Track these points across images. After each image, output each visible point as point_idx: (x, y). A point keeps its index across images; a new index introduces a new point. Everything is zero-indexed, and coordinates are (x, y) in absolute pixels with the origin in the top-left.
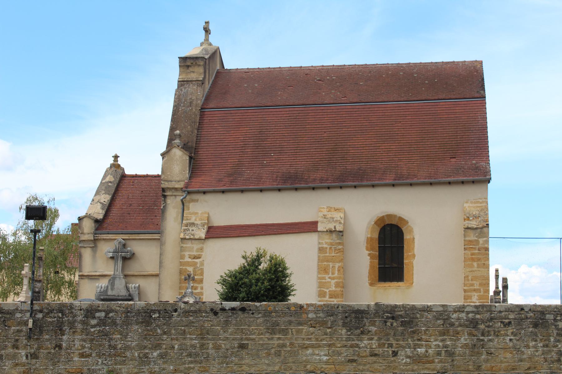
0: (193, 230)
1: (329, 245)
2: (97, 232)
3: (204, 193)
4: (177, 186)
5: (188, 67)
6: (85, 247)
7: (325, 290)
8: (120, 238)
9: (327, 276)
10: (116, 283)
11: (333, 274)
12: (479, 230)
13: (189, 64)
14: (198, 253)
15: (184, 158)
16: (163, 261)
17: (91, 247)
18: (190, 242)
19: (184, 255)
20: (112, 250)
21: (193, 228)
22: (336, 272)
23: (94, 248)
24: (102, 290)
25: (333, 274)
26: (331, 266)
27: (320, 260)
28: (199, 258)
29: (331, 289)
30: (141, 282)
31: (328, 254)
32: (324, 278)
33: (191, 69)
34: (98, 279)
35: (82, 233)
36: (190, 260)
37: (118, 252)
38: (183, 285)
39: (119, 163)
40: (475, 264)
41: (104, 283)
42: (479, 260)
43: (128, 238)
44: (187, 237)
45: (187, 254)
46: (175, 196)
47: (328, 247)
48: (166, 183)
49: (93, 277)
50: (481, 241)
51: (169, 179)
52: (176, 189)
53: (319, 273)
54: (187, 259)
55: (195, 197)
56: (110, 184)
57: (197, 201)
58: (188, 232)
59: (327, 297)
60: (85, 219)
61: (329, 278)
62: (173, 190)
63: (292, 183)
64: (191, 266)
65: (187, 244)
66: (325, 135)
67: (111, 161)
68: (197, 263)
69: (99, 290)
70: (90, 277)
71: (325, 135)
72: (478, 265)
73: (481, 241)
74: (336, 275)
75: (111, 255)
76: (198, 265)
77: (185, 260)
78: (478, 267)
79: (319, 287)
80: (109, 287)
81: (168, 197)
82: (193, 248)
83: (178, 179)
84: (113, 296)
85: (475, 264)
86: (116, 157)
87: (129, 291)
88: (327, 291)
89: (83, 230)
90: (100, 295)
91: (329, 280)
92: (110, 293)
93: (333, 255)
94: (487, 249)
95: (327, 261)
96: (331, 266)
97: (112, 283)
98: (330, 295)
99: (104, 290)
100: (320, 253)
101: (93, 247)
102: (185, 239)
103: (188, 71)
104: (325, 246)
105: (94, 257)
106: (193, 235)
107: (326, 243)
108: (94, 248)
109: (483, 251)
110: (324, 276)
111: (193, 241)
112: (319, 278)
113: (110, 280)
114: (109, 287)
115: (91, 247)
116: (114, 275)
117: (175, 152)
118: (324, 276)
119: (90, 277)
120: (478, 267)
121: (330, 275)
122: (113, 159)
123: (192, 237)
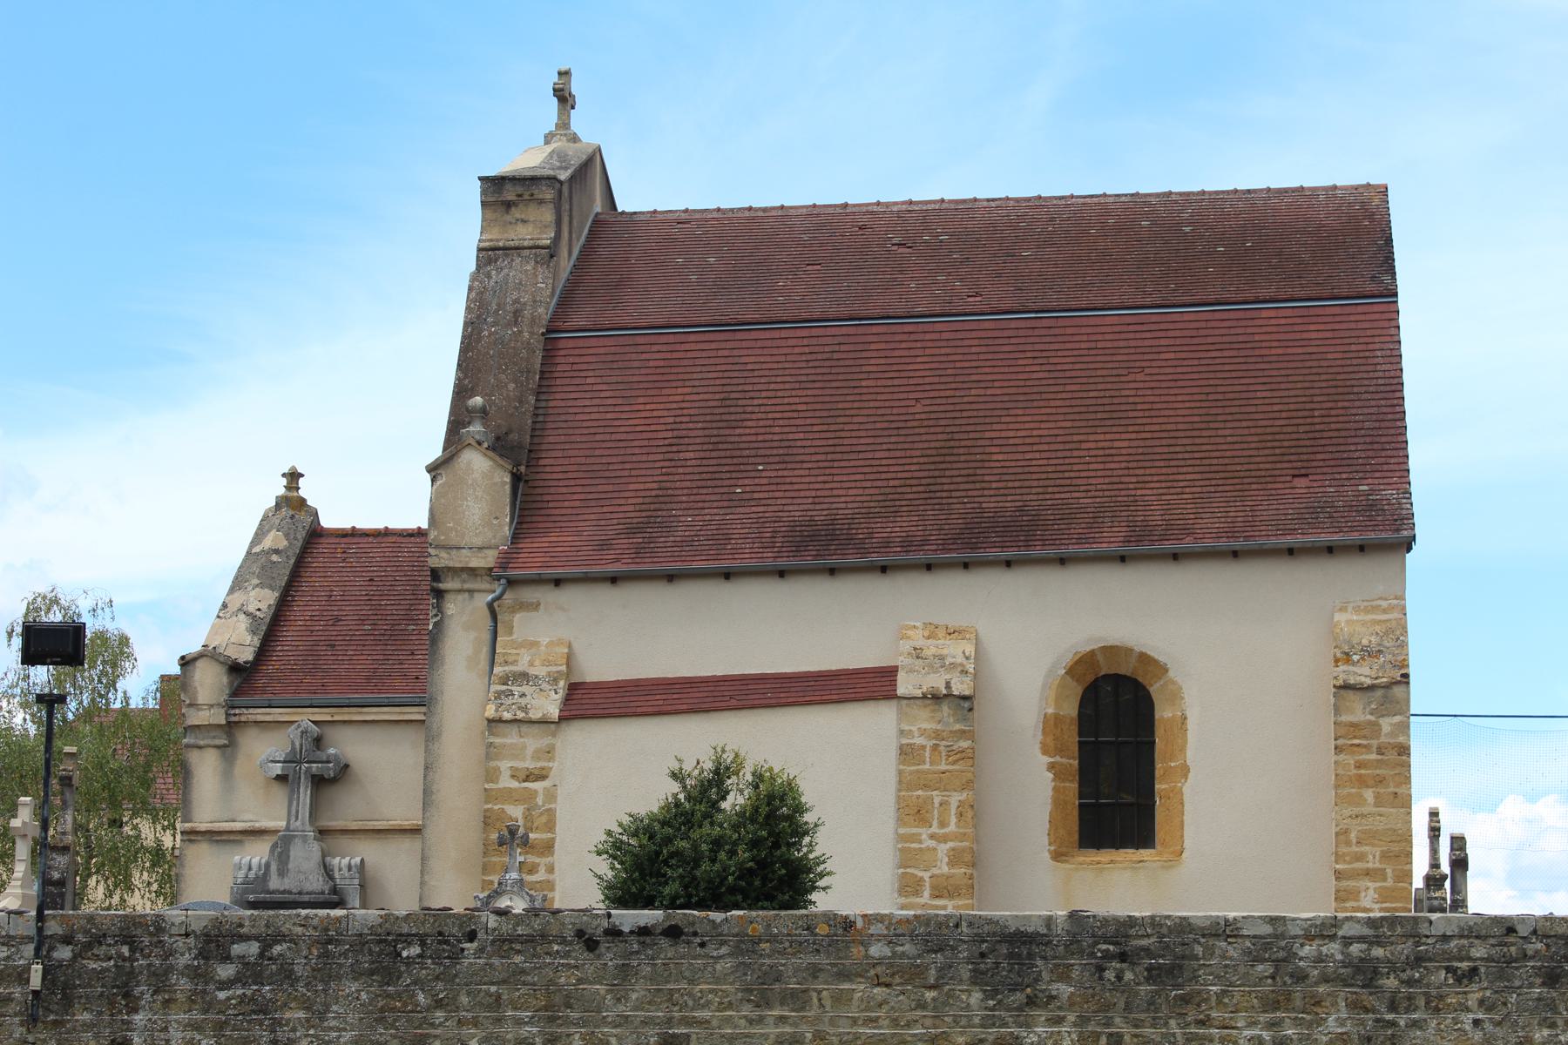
0: (523, 695)
1: (930, 738)
2: (238, 700)
3: (558, 582)
4: (474, 563)
5: (508, 205)
6: (200, 747)
8: (305, 717)
9: (924, 833)
10: (292, 853)
11: (942, 824)
12: (1379, 693)
13: (511, 197)
14: (539, 765)
15: (497, 479)
16: (435, 788)
18: (514, 729)
21: (525, 689)
22: (953, 820)
24: (252, 875)
25: (942, 824)
26: (937, 801)
27: (904, 784)
28: (543, 777)
29: (935, 871)
30: (367, 851)
31: (927, 766)
32: (915, 838)
33: (516, 213)
34: (240, 842)
35: (190, 705)
36: (515, 784)
37: (300, 762)
39: (302, 493)
40: (1369, 795)
41: (256, 854)
42: (1380, 781)
44: (507, 716)
46: (471, 592)
48: (443, 554)
50: (1386, 724)
51: (453, 543)
52: (472, 572)
53: (900, 821)
54: (506, 782)
56: (275, 558)
57: (535, 606)
59: (927, 894)
60: (200, 664)
61: (932, 837)
62: (464, 576)
63: (821, 550)
65: (504, 736)
69: (241, 874)
70: (217, 837)
72: (1377, 796)
74: (952, 827)
75: (277, 769)
76: (540, 801)
77: (501, 785)
78: (1376, 805)
79: (903, 864)
80: (274, 867)
81: (448, 597)
83: (478, 541)
84: (284, 892)
85: (1369, 795)
86: (293, 477)
87: (331, 878)
88: (926, 875)
90: (246, 891)
91: (932, 843)
92: (275, 883)
93: (943, 767)
94: (1404, 750)
95: (926, 787)
96: (937, 801)
97: (280, 854)
98: (933, 887)
100: (903, 762)
101: (225, 746)
102: (500, 721)
103: (508, 218)
104: (918, 741)
105: (227, 775)
106: (525, 709)
107: (923, 732)
108: (228, 750)
109: (1392, 756)
111: (524, 728)
112: (902, 838)
114: (274, 867)
117: (469, 463)
118: (914, 830)
119: (217, 837)
121: (935, 829)
122: (284, 482)
123: (521, 715)
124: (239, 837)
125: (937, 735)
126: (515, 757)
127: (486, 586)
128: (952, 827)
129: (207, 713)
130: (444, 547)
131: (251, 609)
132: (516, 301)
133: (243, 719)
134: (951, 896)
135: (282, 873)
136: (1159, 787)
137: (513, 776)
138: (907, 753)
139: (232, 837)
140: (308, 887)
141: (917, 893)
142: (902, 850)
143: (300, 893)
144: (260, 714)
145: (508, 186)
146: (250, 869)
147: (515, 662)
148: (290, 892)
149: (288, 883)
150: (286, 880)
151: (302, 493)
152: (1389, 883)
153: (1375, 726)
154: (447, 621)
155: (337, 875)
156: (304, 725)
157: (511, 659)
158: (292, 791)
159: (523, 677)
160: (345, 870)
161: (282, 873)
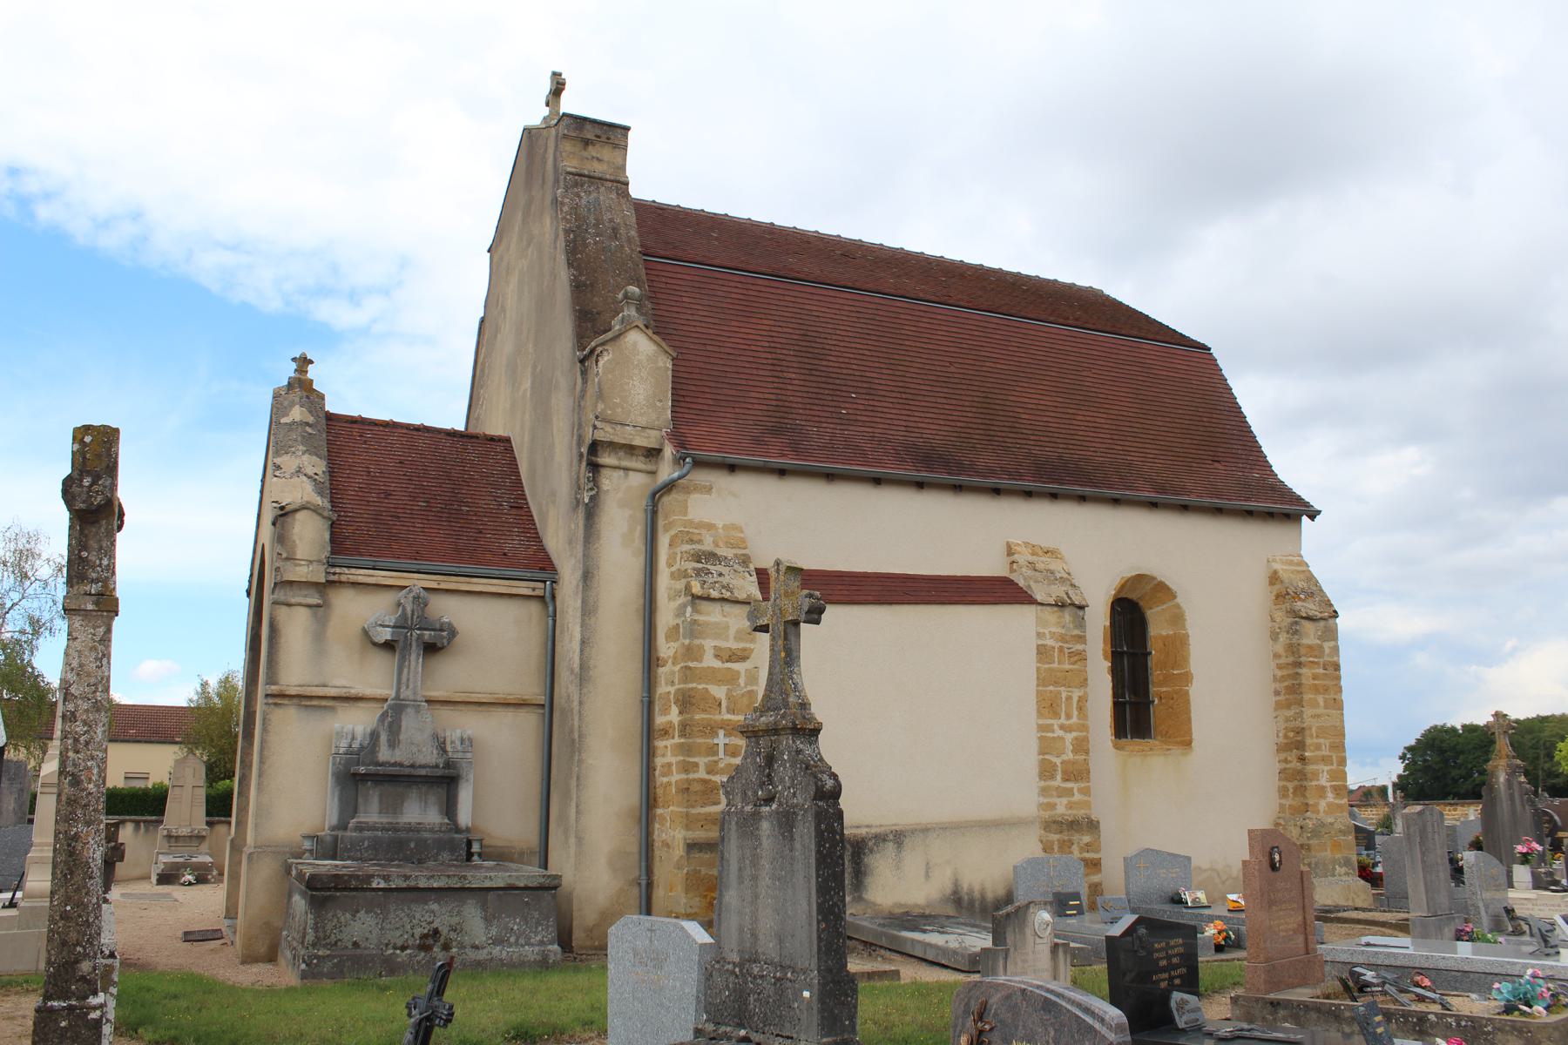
0: (721, 575)
1: (1057, 640)
2: (340, 559)
3: (732, 468)
4: (638, 442)
5: (587, 143)
6: (289, 605)
7: (1055, 760)
8: (418, 582)
9: (1056, 723)
10: (404, 724)
11: (1068, 717)
12: (1322, 623)
13: (590, 136)
14: (742, 645)
15: (661, 364)
16: (592, 663)
17: (309, 606)
18: (717, 607)
19: (701, 647)
20: (391, 620)
21: (720, 568)
22: (1075, 713)
23: (320, 610)
24: (356, 745)
25: (1068, 717)
26: (1064, 695)
27: (1042, 681)
28: (744, 659)
29: (1065, 757)
30: (461, 725)
31: (1055, 665)
32: (1049, 728)
33: (592, 151)
34: (332, 708)
35: (287, 559)
36: (717, 664)
37: (411, 629)
38: (699, 740)
39: (310, 375)
40: (1320, 699)
41: (357, 723)
42: (1326, 690)
43: (435, 585)
44: (714, 594)
45: (709, 644)
46: (626, 469)
47: (1057, 645)
48: (608, 428)
49: (315, 703)
50: (1327, 646)
51: (618, 419)
52: (630, 449)
53: (1040, 714)
54: (710, 661)
55: (703, 477)
56: (309, 430)
57: (709, 490)
58: (710, 579)
59: (1059, 777)
60: (300, 516)
61: (1062, 727)
62: (621, 454)
63: (939, 468)
64: (720, 682)
65: (708, 614)
66: (952, 369)
67: (290, 370)
68: (738, 673)
69: (344, 744)
70: (306, 701)
71: (952, 369)
72: (1326, 701)
73: (1327, 646)
74: (1074, 720)
75: (386, 635)
76: (742, 681)
77: (705, 664)
78: (1326, 707)
79: (1041, 753)
80: (383, 738)
81: (604, 472)
82: (727, 627)
83: (643, 421)
84: (395, 764)
85: (1320, 699)
86: (303, 362)
87: (445, 751)
88: (1058, 761)
89: (294, 546)
90: (348, 763)
91: (1060, 733)
92: (384, 754)
93: (1067, 667)
94: (1337, 667)
95: (1056, 683)
96: (1064, 695)
97: (391, 725)
98: (1064, 772)
99: (362, 748)
100: (1039, 661)
101: (318, 606)
102: (708, 599)
103: (585, 154)
104: (1050, 642)
105: (319, 637)
106: (727, 587)
107: (1053, 635)
108: (320, 610)
109: (1331, 671)
110: (1049, 721)
111: (727, 608)
112: (1041, 728)
113: (384, 715)
114: (383, 738)
115: (309, 606)
116: (397, 697)
117: (635, 344)
118: (1049, 721)
119: (306, 701)
120: (1326, 707)
121: (1063, 720)
122: (294, 366)
123: (727, 595)
124: (330, 703)
125: (1062, 638)
126: (717, 636)
127: (640, 466)
128: (1074, 720)
129: (305, 569)
130: (609, 422)
131: (310, 471)
132: (611, 220)
133: (343, 578)
134: (1076, 780)
135: (393, 744)
136: (1153, 689)
137: (717, 656)
138: (1043, 652)
139: (324, 703)
140: (421, 760)
141: (1052, 777)
142: (1041, 738)
143: (412, 766)
144: (361, 575)
145: (588, 126)
146: (353, 738)
147: (700, 542)
148: (401, 765)
149: (400, 755)
150: (397, 752)
151: (310, 375)
152: (1334, 767)
153: (1321, 647)
154: (602, 496)
155: (449, 748)
156: (416, 590)
157: (695, 538)
158: (403, 659)
159: (712, 557)
160: (458, 743)
161: (393, 744)
